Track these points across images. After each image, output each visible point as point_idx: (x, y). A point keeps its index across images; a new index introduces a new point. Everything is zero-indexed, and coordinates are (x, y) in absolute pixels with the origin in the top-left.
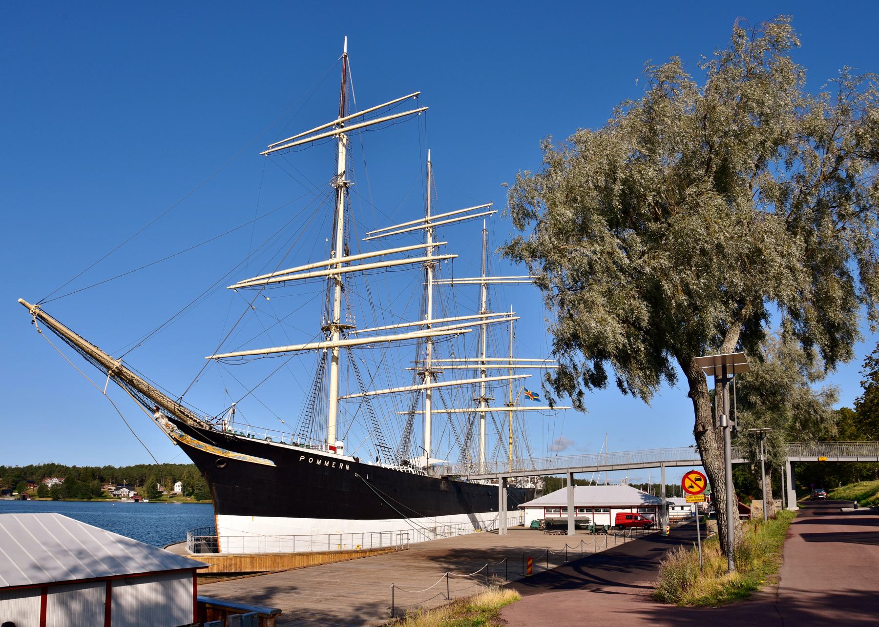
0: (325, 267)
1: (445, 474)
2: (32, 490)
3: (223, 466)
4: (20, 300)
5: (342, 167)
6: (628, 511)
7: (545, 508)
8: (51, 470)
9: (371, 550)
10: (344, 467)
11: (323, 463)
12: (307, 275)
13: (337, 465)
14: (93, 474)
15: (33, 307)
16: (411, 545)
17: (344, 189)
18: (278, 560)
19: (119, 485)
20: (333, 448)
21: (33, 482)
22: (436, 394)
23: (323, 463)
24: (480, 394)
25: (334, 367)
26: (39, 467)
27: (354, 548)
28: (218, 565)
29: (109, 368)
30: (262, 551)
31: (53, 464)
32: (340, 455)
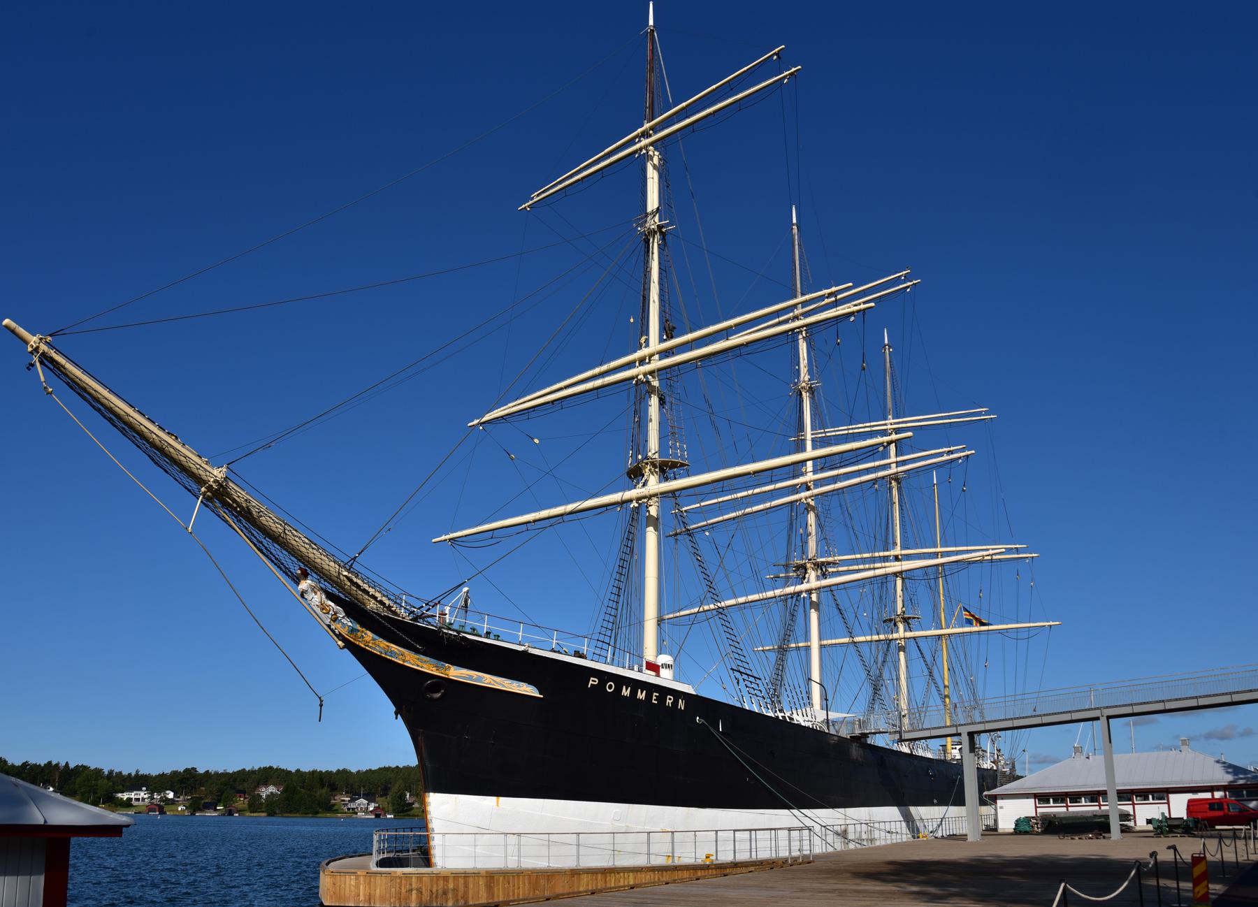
0: (630, 365)
1: (858, 732)
2: (242, 802)
3: (438, 695)
4: (6, 321)
5: (653, 202)
6: (1208, 795)
7: (1035, 796)
8: (267, 775)
9: (735, 865)
10: (675, 703)
11: (634, 693)
12: (598, 382)
13: (662, 699)
14: (321, 779)
15: (33, 340)
16: (817, 857)
17: (657, 236)
18: (542, 882)
19: (355, 795)
20: (653, 667)
21: (244, 792)
22: (826, 596)
23: (634, 693)
24: (895, 610)
25: (651, 536)
26: (253, 772)
27: (700, 859)
28: (420, 891)
29: (200, 481)
30: (512, 864)
31: (271, 768)
32: (666, 679)
